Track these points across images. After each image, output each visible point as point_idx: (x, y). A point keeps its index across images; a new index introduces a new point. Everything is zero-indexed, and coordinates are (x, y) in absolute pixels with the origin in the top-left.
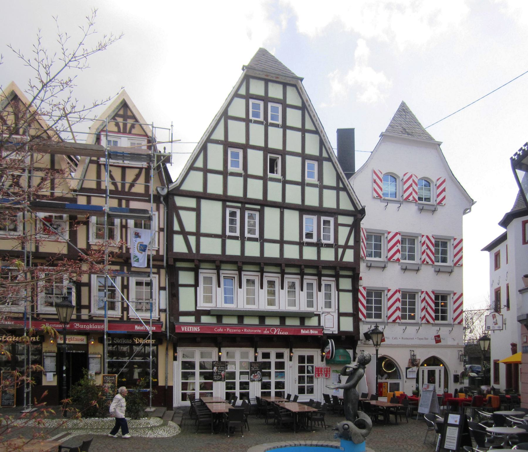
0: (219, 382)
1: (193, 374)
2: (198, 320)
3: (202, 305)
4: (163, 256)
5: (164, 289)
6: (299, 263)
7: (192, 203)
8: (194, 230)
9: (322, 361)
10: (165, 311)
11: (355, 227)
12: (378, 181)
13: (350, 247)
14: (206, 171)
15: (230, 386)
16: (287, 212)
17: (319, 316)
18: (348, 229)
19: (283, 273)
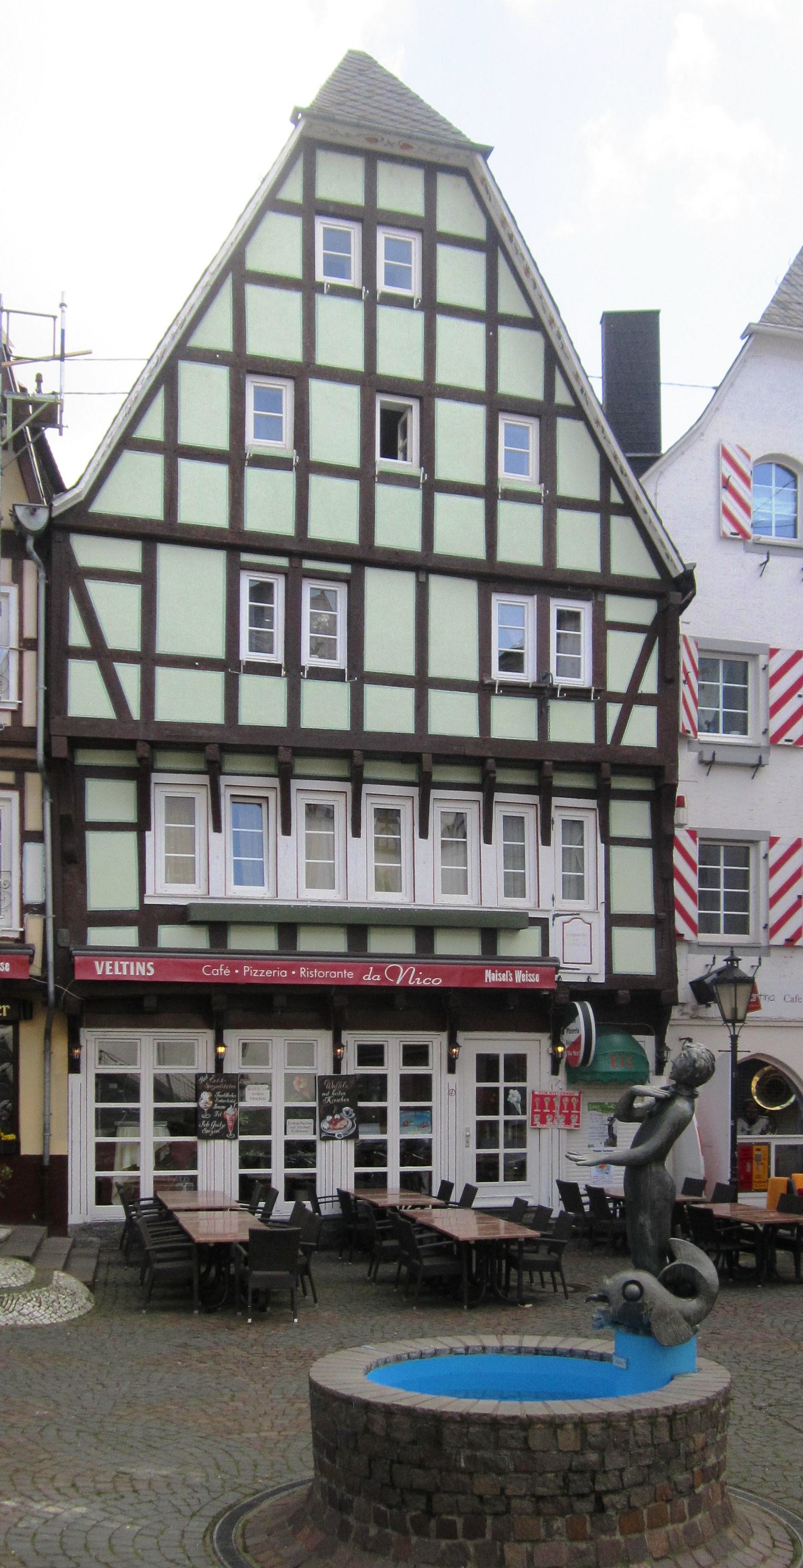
0: (219, 1143)
1: (134, 1116)
2: (148, 939)
3: (163, 890)
4: (34, 730)
5: (37, 837)
6: (478, 753)
7: (127, 555)
8: (134, 644)
9: (555, 1071)
10: (40, 909)
11: (663, 634)
12: (736, 482)
13: (646, 700)
14: (173, 451)
15: (255, 1156)
16: (438, 585)
17: (543, 924)
18: (641, 638)
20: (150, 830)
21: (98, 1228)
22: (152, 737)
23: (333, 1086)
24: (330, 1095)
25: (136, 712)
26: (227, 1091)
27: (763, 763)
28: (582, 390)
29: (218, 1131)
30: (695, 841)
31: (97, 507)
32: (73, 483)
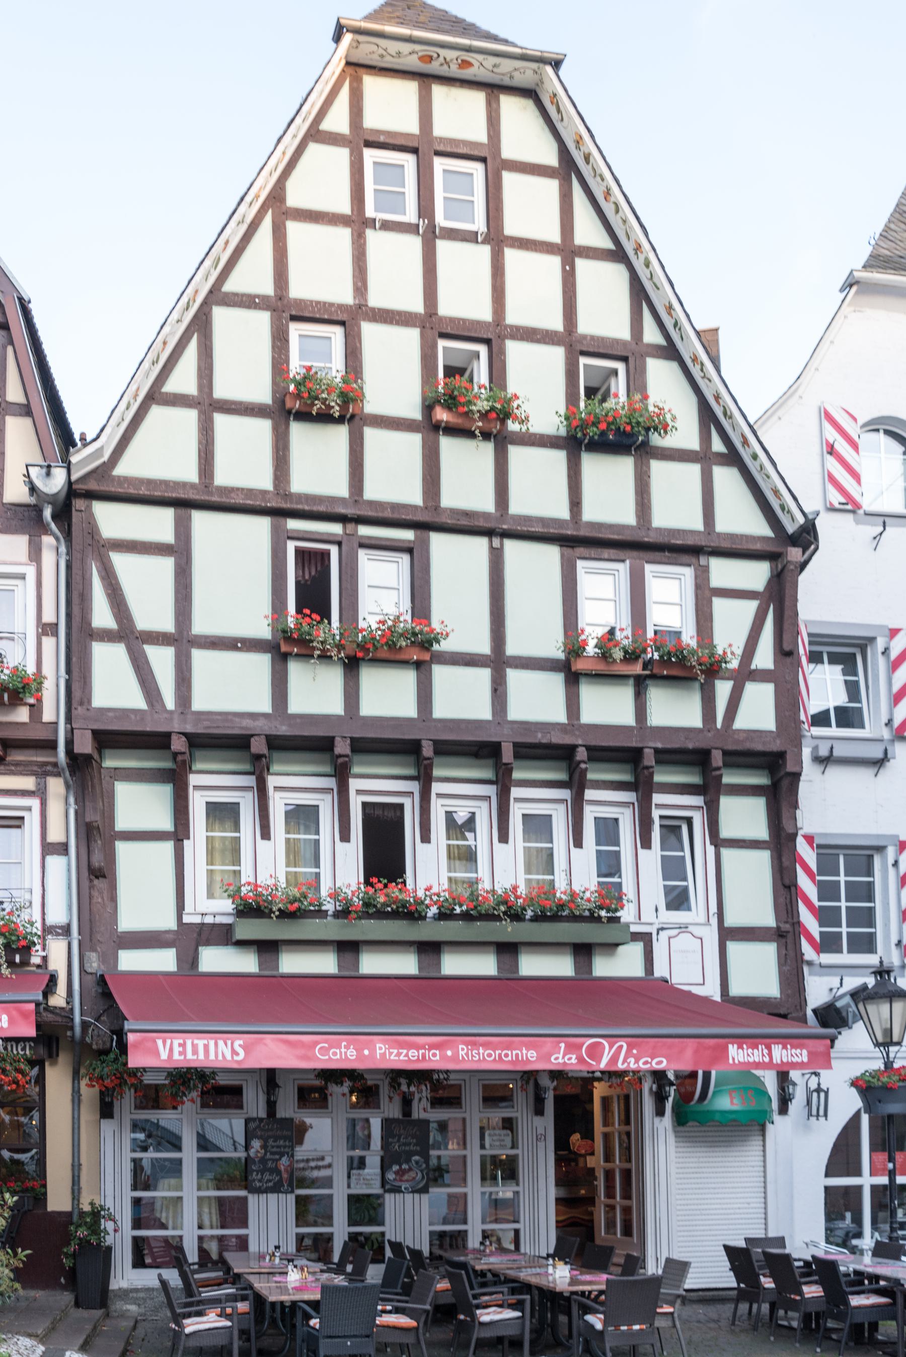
0: (273, 1197)
1: (175, 1168)
2: (189, 960)
5: (62, 849)
6: (568, 740)
7: (158, 524)
8: (167, 624)
10: (66, 930)
11: (779, 597)
12: (842, 447)
14: (208, 405)
16: (512, 549)
17: (646, 939)
18: (753, 605)
19: (503, 783)
20: (188, 838)
21: (135, 1295)
22: (189, 729)
23: (402, 1131)
24: (399, 1141)
25: (170, 702)
26: (280, 1138)
27: (889, 756)
28: (676, 325)
29: (270, 1184)
30: (813, 848)
31: (122, 469)
32: (94, 436)
